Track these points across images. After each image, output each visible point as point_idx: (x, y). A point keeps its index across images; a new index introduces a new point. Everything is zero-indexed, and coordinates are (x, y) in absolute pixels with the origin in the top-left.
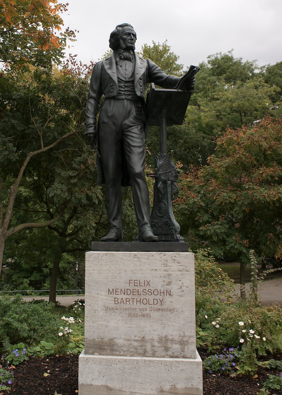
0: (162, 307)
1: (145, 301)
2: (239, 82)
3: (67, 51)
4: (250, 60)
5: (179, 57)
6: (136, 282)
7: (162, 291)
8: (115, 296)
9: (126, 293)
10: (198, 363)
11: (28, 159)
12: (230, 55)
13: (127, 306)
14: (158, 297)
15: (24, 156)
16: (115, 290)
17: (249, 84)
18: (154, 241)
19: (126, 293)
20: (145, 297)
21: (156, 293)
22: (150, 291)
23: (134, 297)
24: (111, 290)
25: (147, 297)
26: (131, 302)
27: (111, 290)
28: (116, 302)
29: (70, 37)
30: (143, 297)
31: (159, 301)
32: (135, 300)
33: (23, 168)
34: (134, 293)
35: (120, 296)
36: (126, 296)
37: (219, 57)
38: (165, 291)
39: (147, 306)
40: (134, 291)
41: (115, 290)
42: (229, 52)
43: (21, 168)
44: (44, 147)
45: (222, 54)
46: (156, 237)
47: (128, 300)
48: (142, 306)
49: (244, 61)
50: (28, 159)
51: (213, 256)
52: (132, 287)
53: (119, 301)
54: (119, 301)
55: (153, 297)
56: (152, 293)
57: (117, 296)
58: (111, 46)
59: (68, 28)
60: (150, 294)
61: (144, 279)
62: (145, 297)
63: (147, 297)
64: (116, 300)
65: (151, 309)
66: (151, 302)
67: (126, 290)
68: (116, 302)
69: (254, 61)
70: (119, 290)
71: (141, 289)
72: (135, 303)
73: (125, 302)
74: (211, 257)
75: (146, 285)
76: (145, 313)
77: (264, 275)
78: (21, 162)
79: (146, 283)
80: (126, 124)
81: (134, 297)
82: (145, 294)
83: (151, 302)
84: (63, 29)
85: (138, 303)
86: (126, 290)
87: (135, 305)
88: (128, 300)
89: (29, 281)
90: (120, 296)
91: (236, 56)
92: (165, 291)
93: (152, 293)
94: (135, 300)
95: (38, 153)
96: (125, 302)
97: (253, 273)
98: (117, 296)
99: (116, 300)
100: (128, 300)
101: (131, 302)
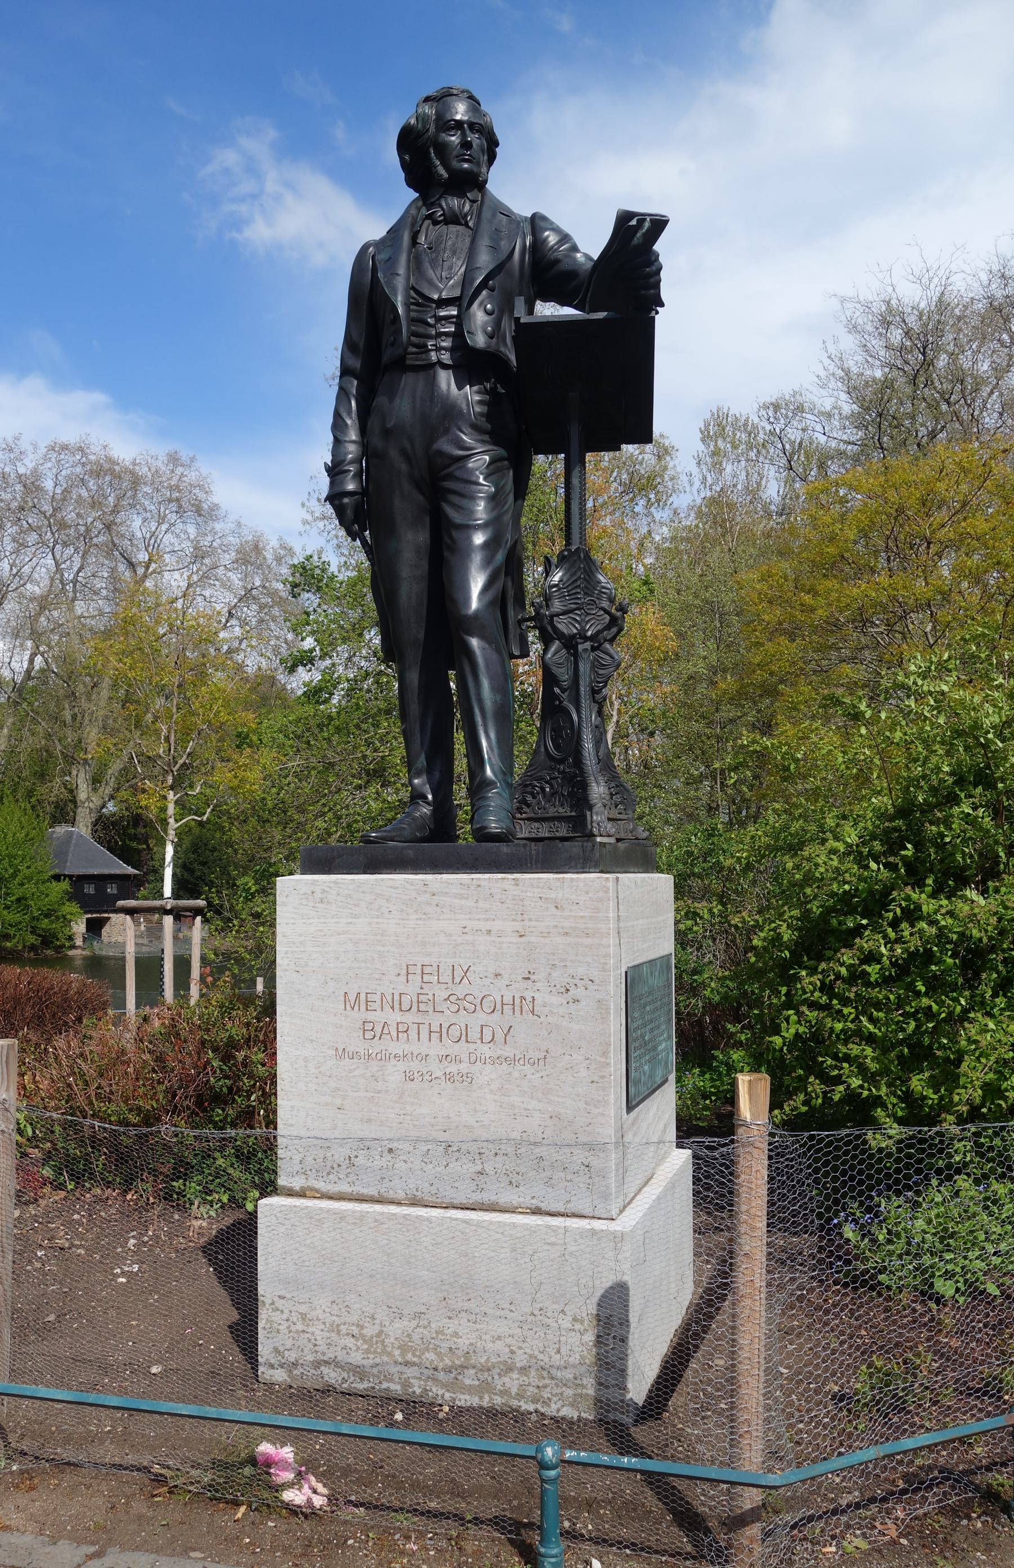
0: (508, 1052)
7: (508, 999)
16: (363, 996)
26: (413, 1034)
27: (352, 997)
34: (422, 1007)
36: (397, 1017)
38: (517, 1001)
39: (462, 1049)
40: (427, 970)
41: (363, 996)
57: (371, 1016)
58: (411, 182)
61: (451, 961)
66: (474, 1034)
67: (397, 997)
70: (377, 998)
76: (453, 1068)
80: (440, 453)
87: (435, 1049)
92: (517, 1001)
96: (394, 1034)
101: (413, 1034)
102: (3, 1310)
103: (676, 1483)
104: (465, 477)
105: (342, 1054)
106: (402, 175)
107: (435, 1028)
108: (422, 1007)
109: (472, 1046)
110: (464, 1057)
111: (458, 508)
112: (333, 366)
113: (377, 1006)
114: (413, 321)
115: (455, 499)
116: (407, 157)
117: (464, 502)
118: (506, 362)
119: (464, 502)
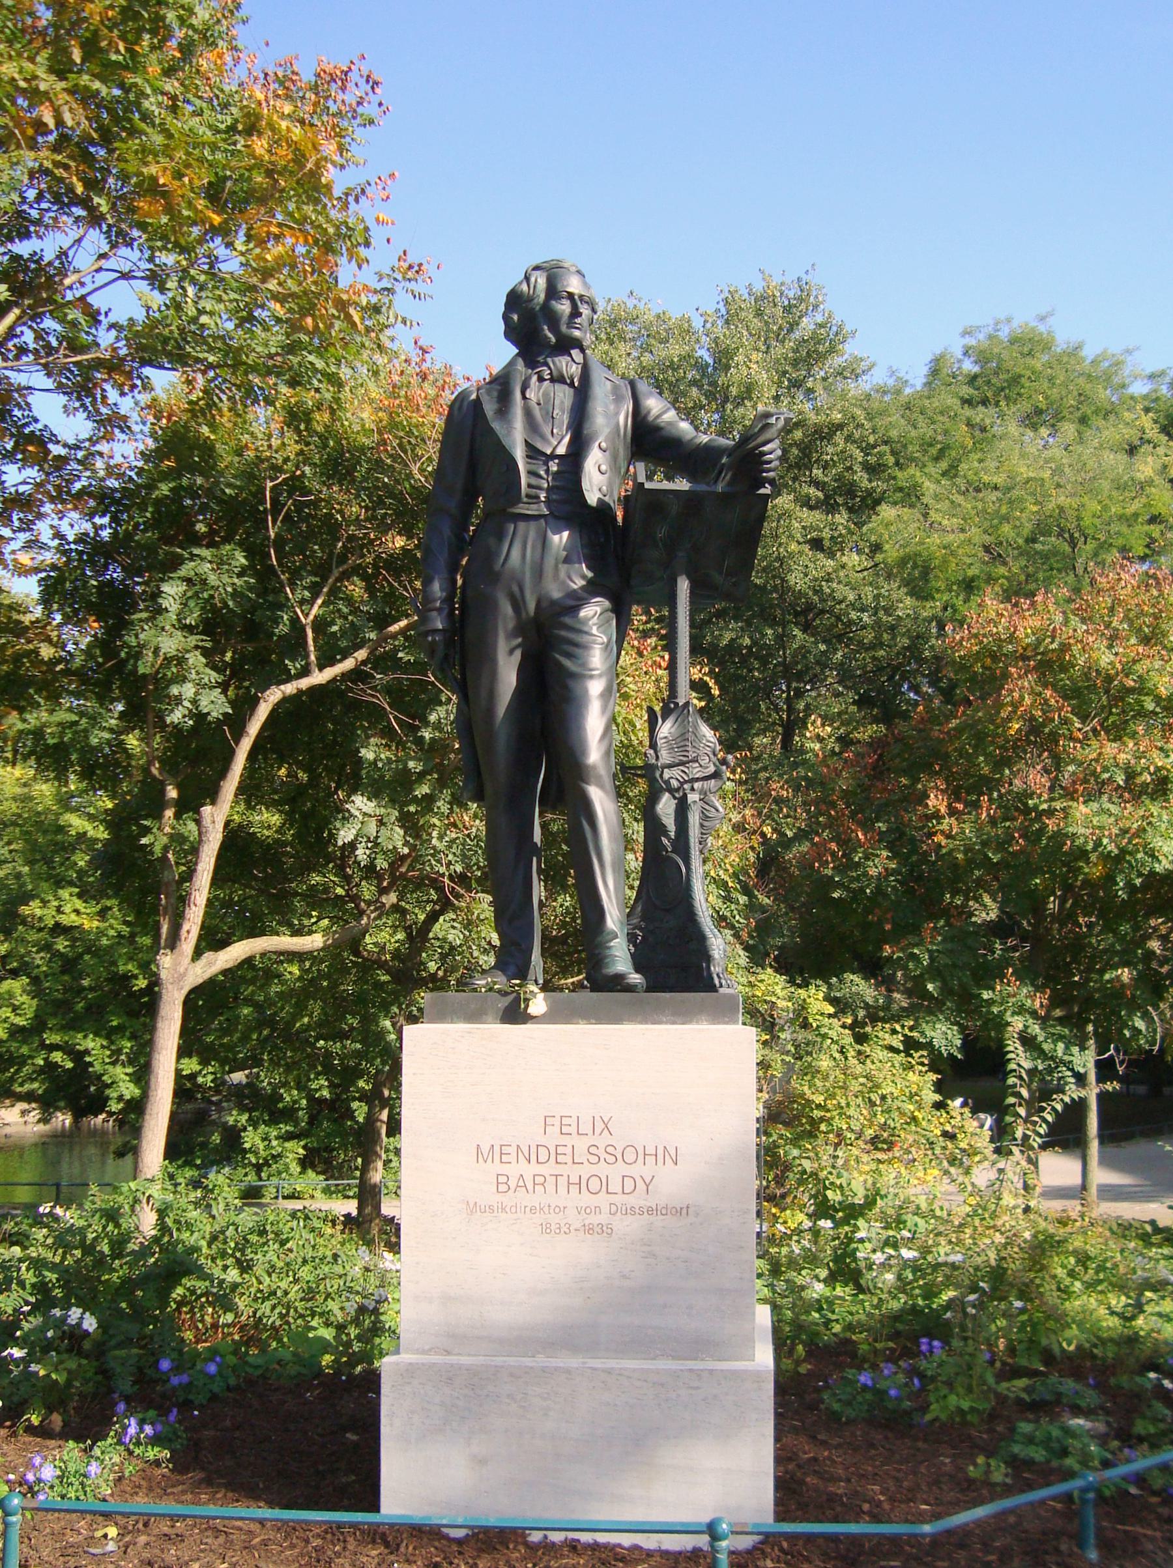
1: (594, 1184)
2: (1069, 429)
3: (401, 340)
4: (1115, 348)
5: (854, 333)
6: (565, 1121)
8: (499, 1168)
9: (533, 1158)
10: (757, 1375)
11: (263, 711)
12: (1042, 328)
13: (537, 1198)
14: (636, 1170)
15: (244, 706)
16: (497, 1149)
17: (1115, 432)
18: (630, 989)
19: (533, 1158)
20: (594, 1170)
21: (630, 1157)
22: (610, 1149)
23: (559, 1170)
24: (485, 1149)
25: (602, 1169)
27: (485, 1149)
28: (503, 1188)
29: (412, 286)
30: (585, 1171)
31: (639, 1181)
32: (562, 1181)
33: (246, 745)
34: (560, 1159)
35: (514, 1170)
36: (535, 1168)
37: (1004, 334)
39: (602, 1200)
40: (560, 1150)
41: (497, 1149)
42: (1042, 319)
43: (237, 743)
44: (321, 670)
45: (1015, 324)
46: (636, 978)
47: (541, 1179)
48: (586, 1199)
49: (1089, 352)
50: (263, 711)
51: (925, 1053)
52: (553, 1138)
53: (512, 1184)
54: (512, 1184)
55: (621, 1168)
56: (615, 1156)
57: (505, 1169)
59: (405, 253)
60: (611, 1159)
62: (594, 1170)
63: (602, 1169)
64: (502, 1179)
65: (614, 1208)
66: (615, 1186)
67: (533, 1150)
68: (503, 1188)
69: (1128, 352)
70: (513, 1150)
71: (582, 1144)
72: (562, 1189)
73: (530, 1186)
74: (916, 1055)
75: (598, 1131)
77: (1054, 1109)
78: (237, 722)
79: (599, 1126)
81: (559, 1170)
82: (594, 1159)
83: (615, 1186)
84: (380, 257)
85: (574, 1189)
86: (533, 1150)
88: (539, 1182)
89: (304, 1147)
90: (514, 1170)
91: (1064, 334)
93: (615, 1156)
94: (562, 1181)
95: (300, 692)
96: (530, 1186)
97: (1011, 1100)
98: (505, 1169)
99: (501, 1183)
100: (539, 1182)
102: (72, 1564)
103: (445, 1530)
104: (578, 626)
105: (473, 1208)
106: (504, 299)
107: (576, 1180)
108: (560, 1159)
109: (612, 1198)
110: (605, 1209)
111: (569, 656)
112: (772, 1393)
113: (513, 1158)
114: (530, 486)
115: (566, 647)
116: (515, 317)
117: (577, 651)
118: (615, 518)
119: (577, 651)
